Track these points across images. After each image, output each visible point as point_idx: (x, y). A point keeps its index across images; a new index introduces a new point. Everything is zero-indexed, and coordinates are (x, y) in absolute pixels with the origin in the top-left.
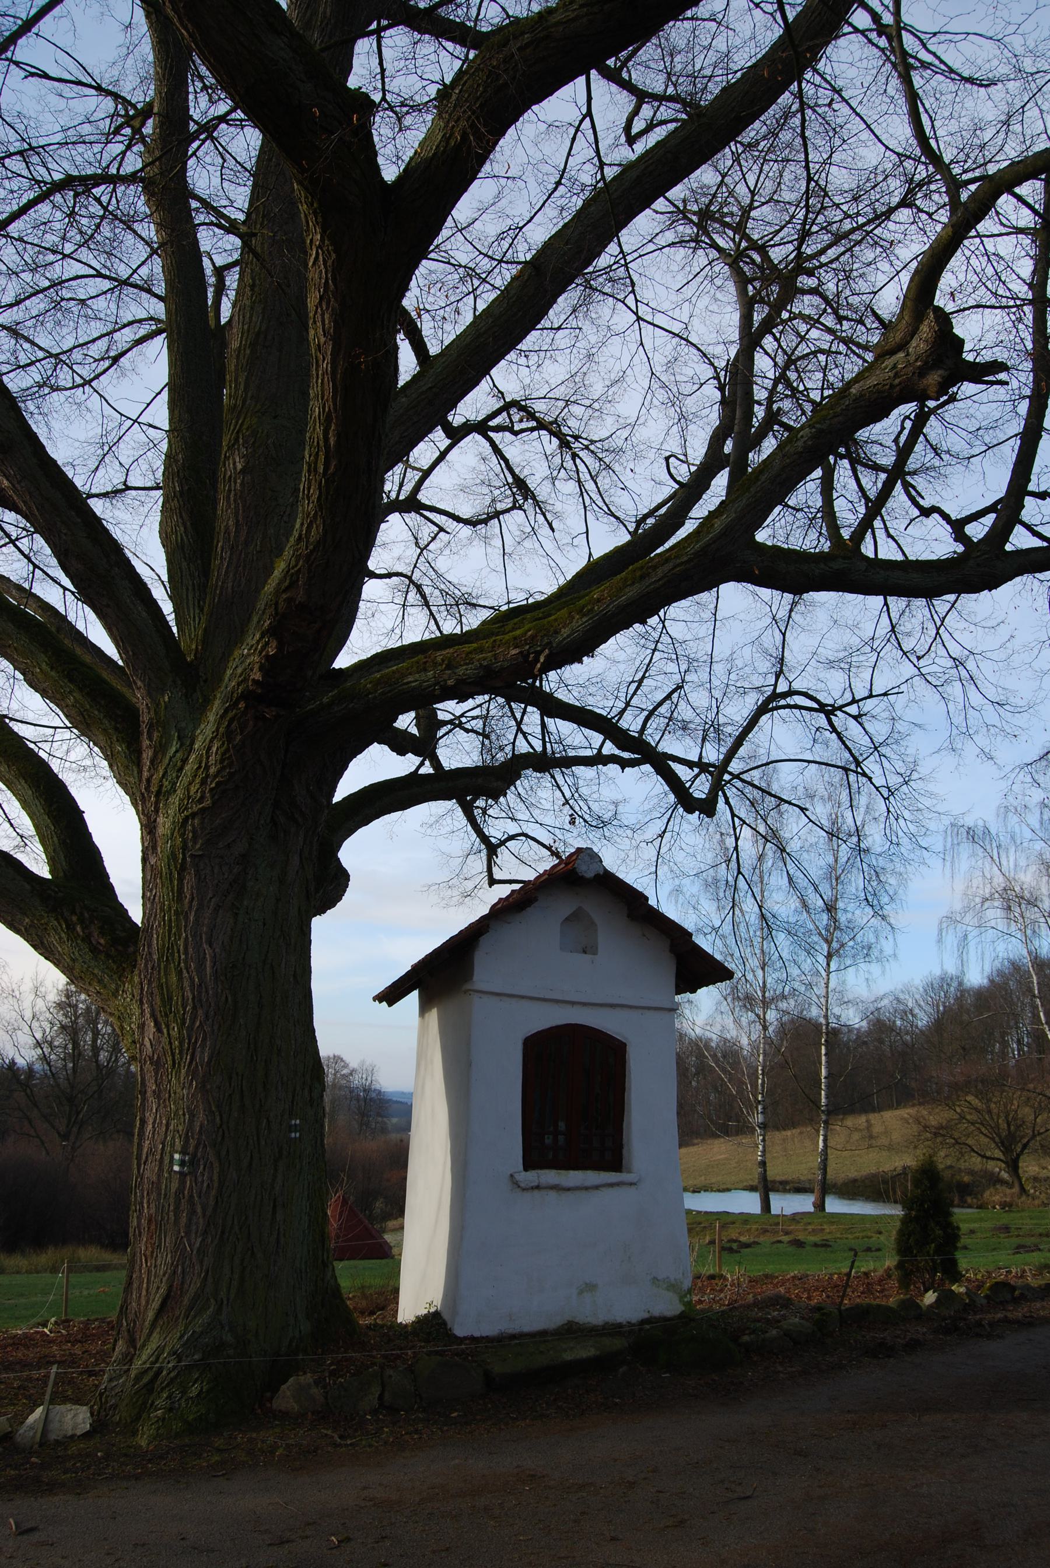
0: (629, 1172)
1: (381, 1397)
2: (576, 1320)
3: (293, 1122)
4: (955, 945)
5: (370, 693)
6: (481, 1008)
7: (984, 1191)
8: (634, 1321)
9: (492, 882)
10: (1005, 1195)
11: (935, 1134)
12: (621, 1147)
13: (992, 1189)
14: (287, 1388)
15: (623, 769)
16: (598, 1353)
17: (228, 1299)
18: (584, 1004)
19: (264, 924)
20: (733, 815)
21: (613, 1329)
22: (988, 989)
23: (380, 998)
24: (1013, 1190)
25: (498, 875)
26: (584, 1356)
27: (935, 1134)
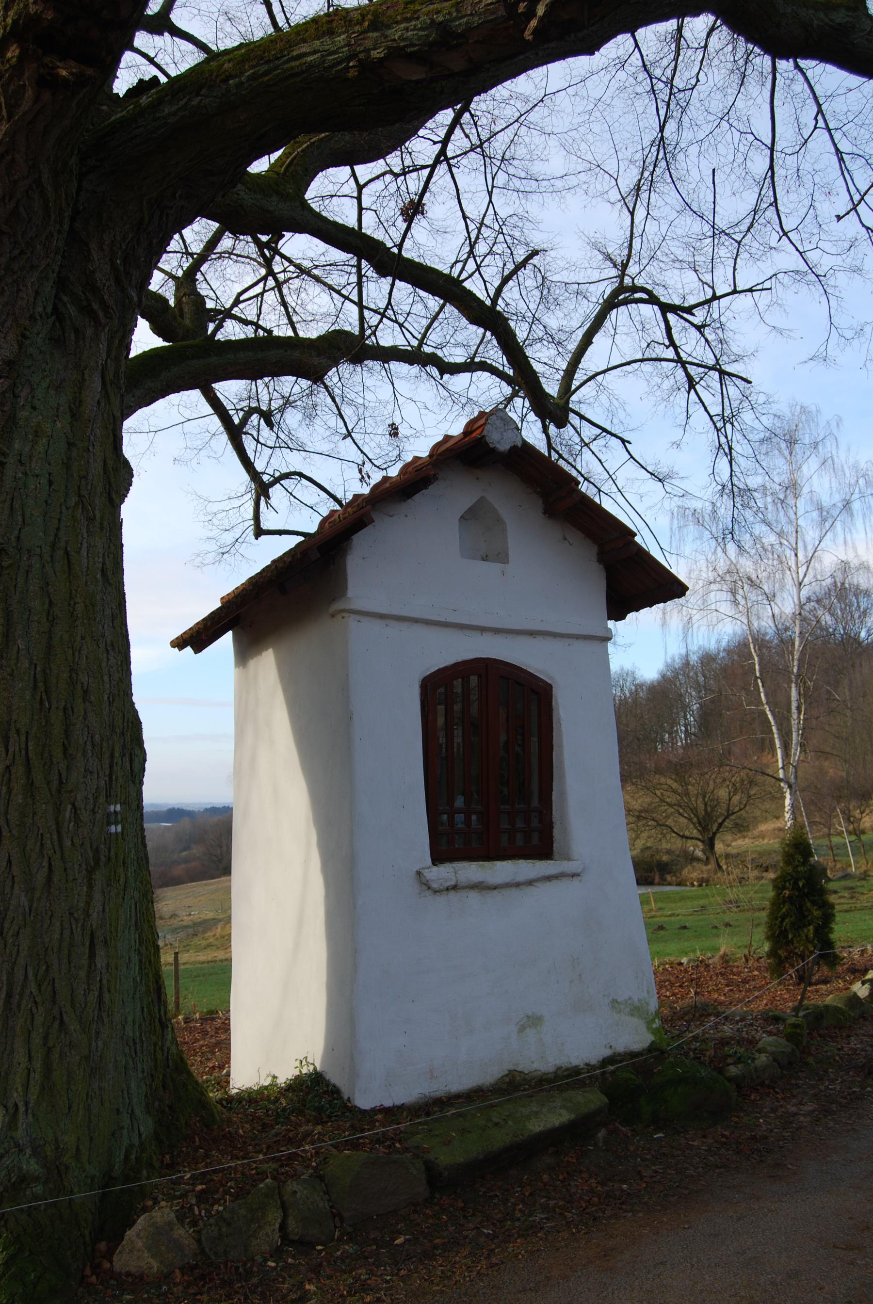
0: (568, 858)
1: (283, 1227)
2: (520, 1068)
3: (112, 808)
4: (681, 627)
5: (230, 77)
6: (362, 635)
7: (682, 869)
9: (259, 532)
10: (702, 872)
11: (638, 817)
12: (550, 826)
13: (689, 867)
14: (136, 1234)
16: (573, 1116)
17: (26, 1104)
18: (497, 631)
19: (50, 483)
21: (568, 1079)
22: (659, 682)
23: (180, 643)
24: (709, 867)
25: (265, 525)
26: (557, 1124)
27: (638, 817)
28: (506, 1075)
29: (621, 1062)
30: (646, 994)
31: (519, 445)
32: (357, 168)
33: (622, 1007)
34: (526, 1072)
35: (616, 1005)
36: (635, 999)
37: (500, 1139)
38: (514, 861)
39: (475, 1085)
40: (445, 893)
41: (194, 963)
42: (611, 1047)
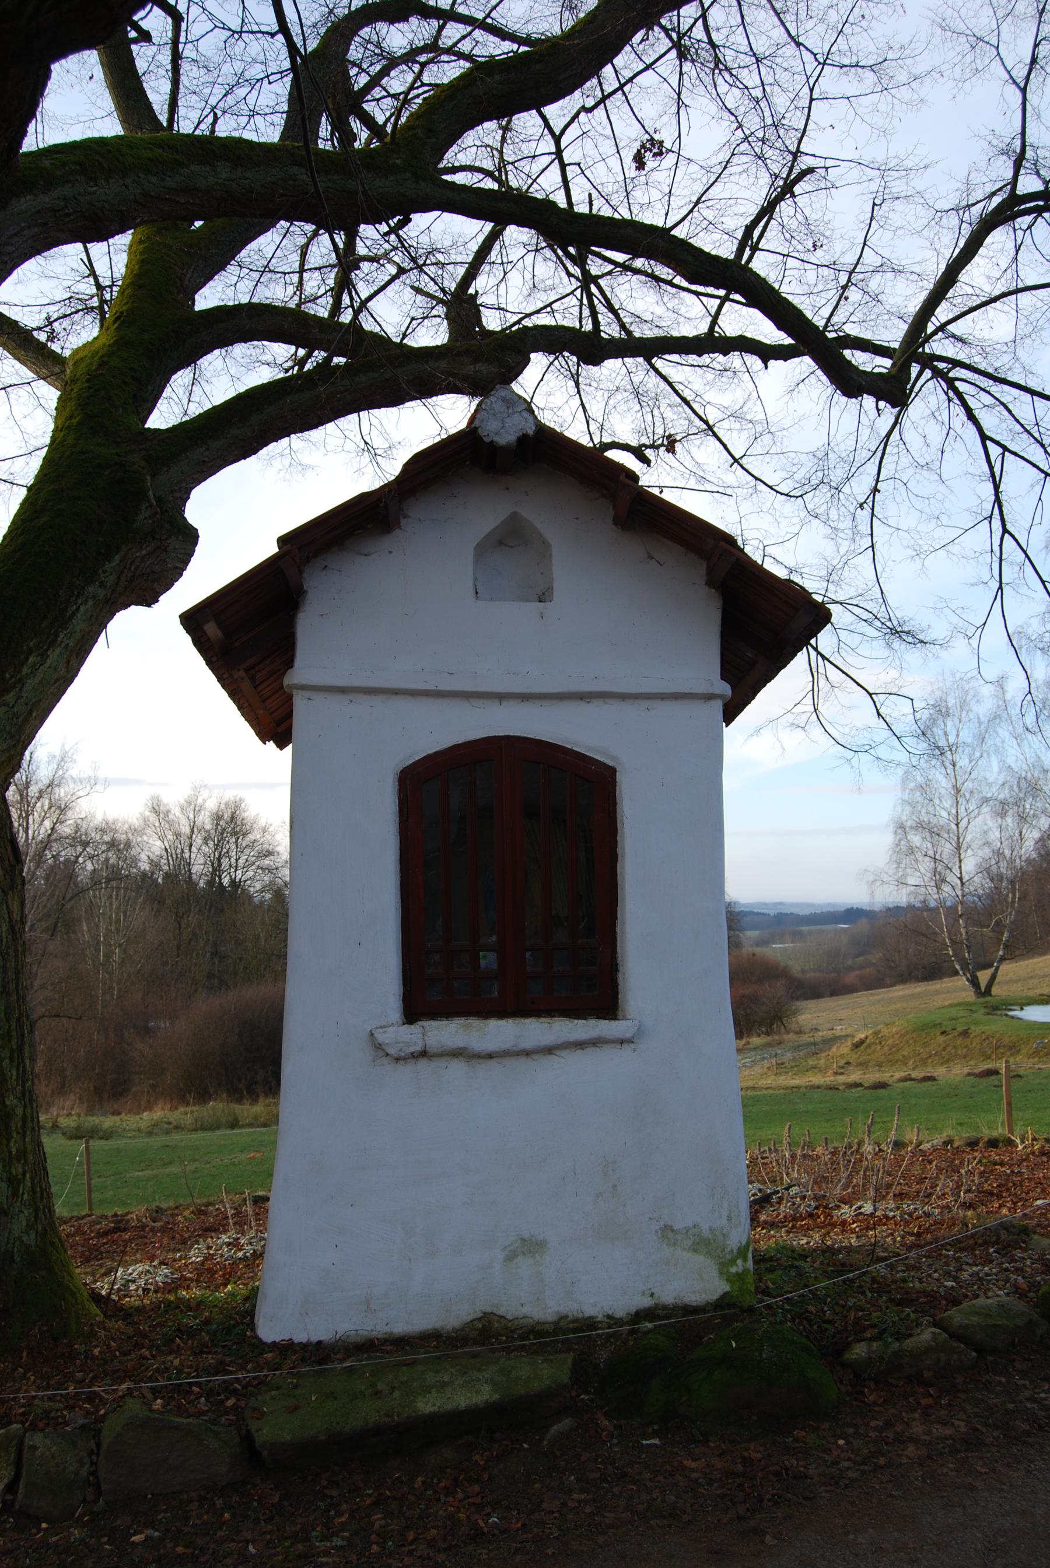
0: (625, 1018)
2: (501, 1311)
8: (620, 1313)
15: (765, 363)
18: (525, 697)
20: (984, 438)
21: (572, 1336)
28: (479, 1319)
29: (668, 1318)
30: (724, 1221)
31: (531, 432)
32: (549, 110)
33: (679, 1237)
34: (510, 1317)
35: (670, 1235)
36: (705, 1228)
37: (367, 1413)
38: (519, 1020)
39: (430, 1327)
40: (413, 1061)
41: (780, 1088)
42: (652, 1295)
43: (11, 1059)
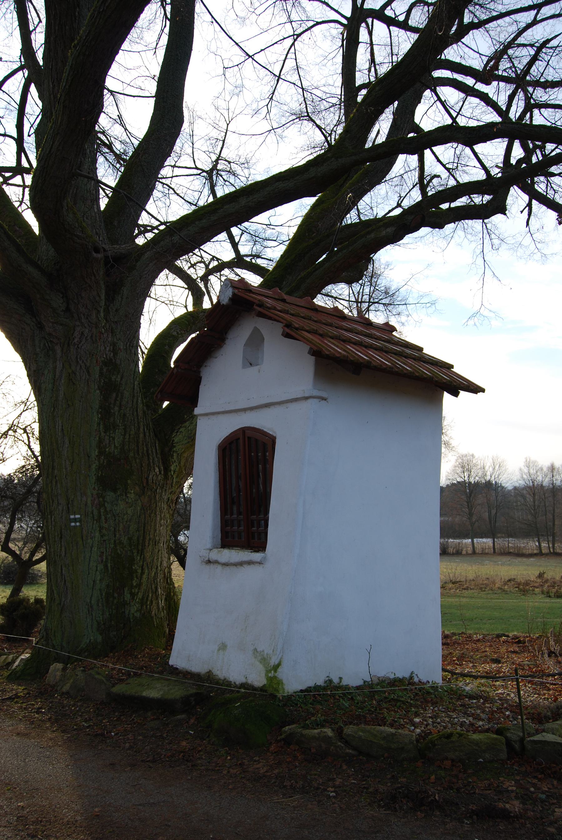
43: (138, 553)
